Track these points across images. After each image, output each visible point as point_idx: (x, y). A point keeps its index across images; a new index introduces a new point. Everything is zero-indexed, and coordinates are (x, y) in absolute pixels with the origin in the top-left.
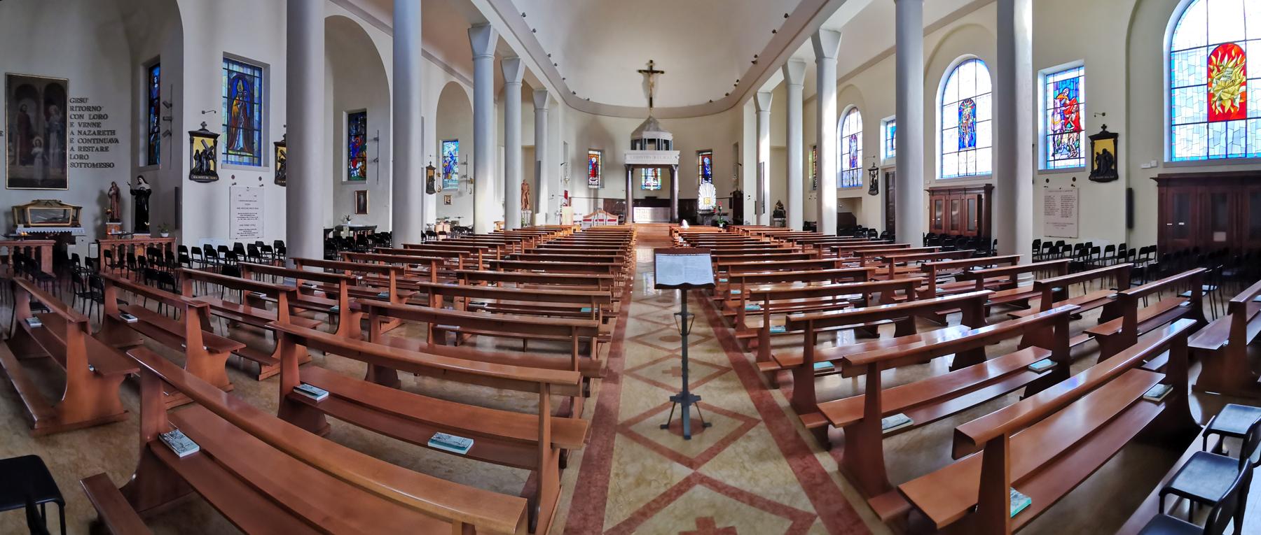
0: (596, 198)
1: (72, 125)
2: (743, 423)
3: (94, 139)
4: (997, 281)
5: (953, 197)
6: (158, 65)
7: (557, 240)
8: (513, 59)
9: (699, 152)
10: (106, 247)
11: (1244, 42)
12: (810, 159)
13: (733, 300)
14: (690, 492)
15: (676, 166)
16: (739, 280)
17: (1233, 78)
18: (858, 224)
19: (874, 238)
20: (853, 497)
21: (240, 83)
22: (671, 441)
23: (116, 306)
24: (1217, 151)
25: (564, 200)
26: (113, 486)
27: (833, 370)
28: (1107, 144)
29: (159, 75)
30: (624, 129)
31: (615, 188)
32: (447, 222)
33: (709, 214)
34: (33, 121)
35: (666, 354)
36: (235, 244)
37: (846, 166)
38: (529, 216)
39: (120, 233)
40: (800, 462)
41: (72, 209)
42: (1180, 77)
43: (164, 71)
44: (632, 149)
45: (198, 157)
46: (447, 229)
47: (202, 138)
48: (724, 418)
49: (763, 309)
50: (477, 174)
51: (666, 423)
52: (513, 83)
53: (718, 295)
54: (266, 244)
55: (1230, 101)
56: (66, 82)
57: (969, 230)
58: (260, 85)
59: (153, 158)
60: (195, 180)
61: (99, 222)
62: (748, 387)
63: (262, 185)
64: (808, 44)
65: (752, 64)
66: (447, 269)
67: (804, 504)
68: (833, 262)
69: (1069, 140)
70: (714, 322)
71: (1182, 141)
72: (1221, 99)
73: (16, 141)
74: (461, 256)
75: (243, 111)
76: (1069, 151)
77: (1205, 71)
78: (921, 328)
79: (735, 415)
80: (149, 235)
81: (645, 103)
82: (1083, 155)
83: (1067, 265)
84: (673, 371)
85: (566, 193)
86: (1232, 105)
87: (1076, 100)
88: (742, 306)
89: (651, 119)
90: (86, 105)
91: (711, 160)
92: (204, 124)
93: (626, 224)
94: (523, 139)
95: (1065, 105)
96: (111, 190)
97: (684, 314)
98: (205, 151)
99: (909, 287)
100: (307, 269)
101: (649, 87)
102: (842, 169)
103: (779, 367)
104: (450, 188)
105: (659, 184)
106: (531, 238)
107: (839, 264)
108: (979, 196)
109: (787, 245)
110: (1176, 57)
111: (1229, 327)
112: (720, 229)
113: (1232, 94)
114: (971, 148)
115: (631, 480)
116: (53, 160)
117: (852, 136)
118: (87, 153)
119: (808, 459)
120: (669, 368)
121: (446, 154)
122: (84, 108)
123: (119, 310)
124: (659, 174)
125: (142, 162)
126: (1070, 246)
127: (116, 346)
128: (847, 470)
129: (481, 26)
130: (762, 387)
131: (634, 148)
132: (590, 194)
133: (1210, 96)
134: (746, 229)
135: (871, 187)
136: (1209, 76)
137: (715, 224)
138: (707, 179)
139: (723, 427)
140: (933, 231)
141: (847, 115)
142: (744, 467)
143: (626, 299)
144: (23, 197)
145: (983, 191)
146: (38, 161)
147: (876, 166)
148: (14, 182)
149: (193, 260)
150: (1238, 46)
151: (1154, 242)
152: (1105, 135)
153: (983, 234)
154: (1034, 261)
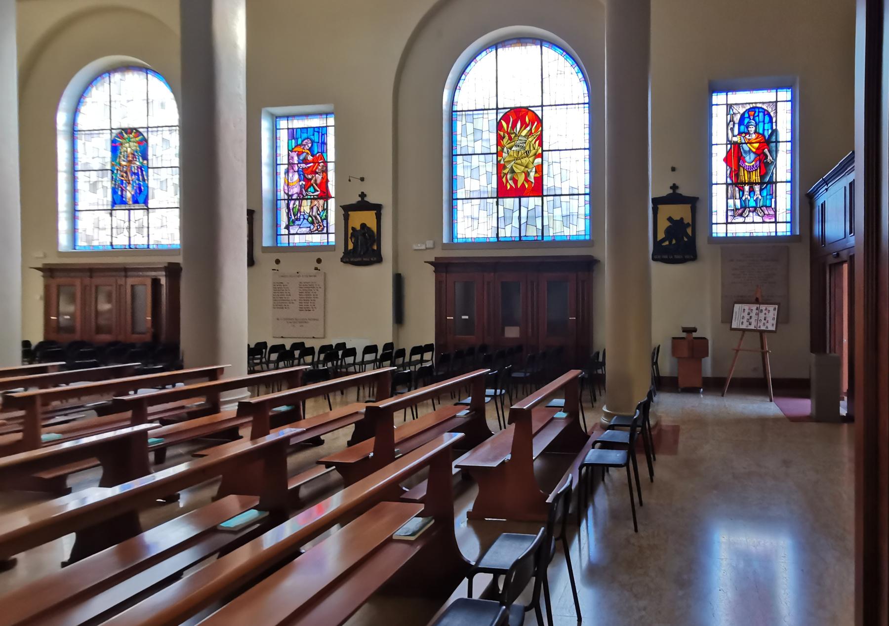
4: (183, 407)
5: (97, 280)
11: (540, 108)
17: (527, 148)
24: (508, 232)
28: (368, 218)
42: (463, 142)
55: (523, 174)
57: (133, 332)
69: (312, 208)
71: (466, 219)
72: (512, 171)
76: (312, 223)
77: (493, 138)
82: (332, 229)
83: (300, 375)
86: (526, 180)
87: (322, 157)
95: (305, 161)
108: (156, 282)
110: (459, 118)
111: (512, 439)
113: (526, 167)
114: (137, 206)
126: (312, 349)
133: (500, 167)
136: (498, 144)
140: (53, 337)
145: (164, 273)
150: (533, 112)
151: (431, 339)
152: (363, 205)
154: (250, 372)
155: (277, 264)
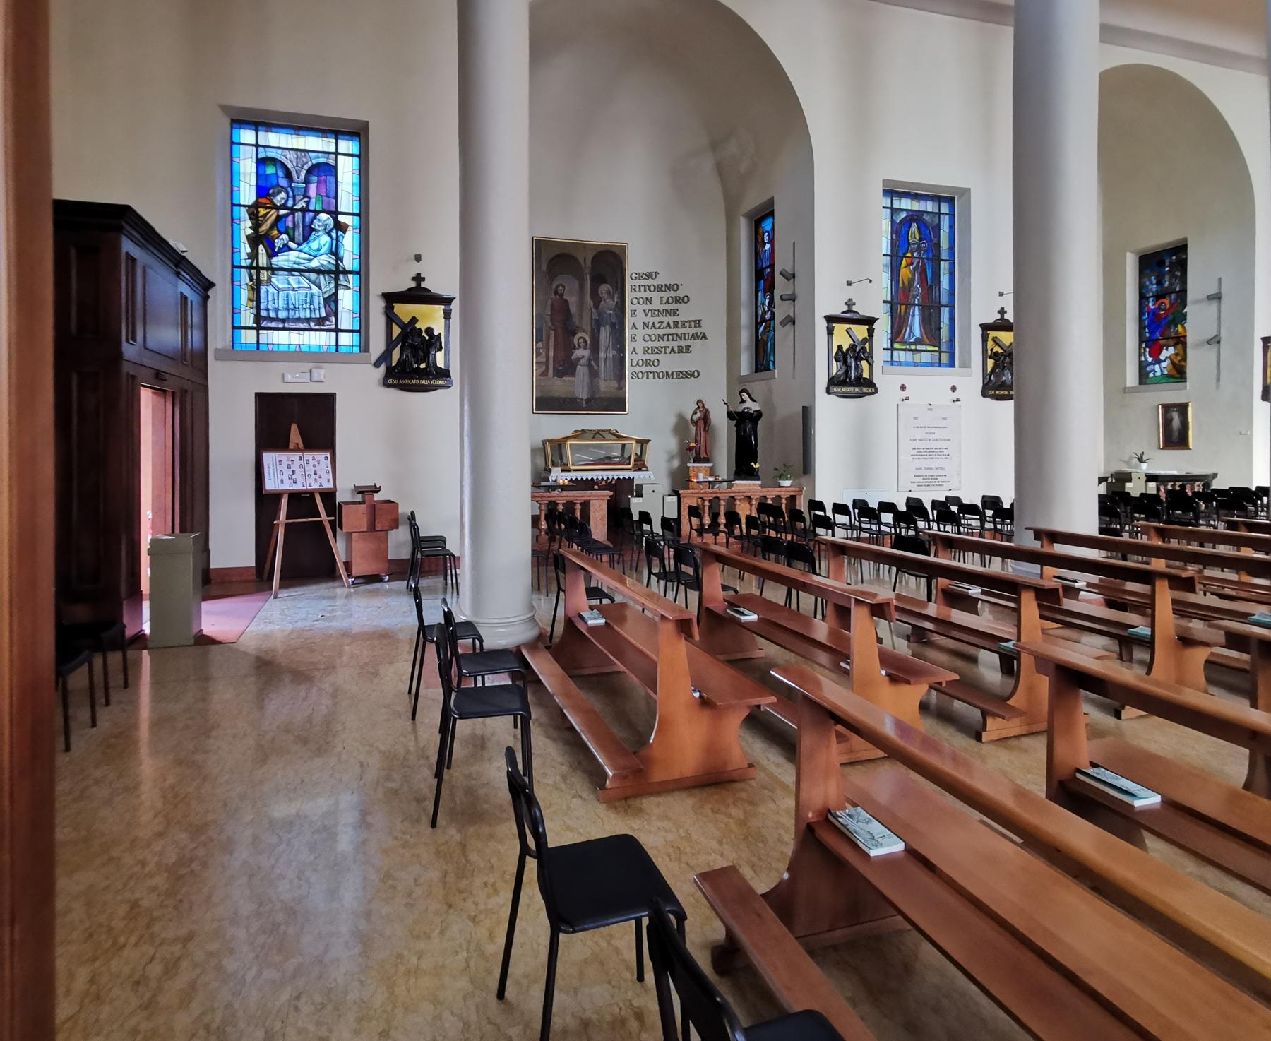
1: (634, 313)
3: (668, 335)
6: (772, 214)
10: (689, 501)
18: (1127, 707)
21: (914, 227)
23: (721, 595)
26: (751, 890)
29: (773, 228)
34: (573, 309)
36: (908, 500)
39: (711, 479)
41: (634, 443)
43: (781, 223)
45: (842, 356)
47: (847, 326)
54: (965, 501)
56: (623, 249)
58: (952, 227)
59: (763, 358)
60: (836, 394)
61: (676, 463)
63: (958, 400)
73: (548, 338)
75: (920, 274)
80: (759, 482)
90: (655, 282)
92: (850, 304)
96: (695, 413)
98: (852, 347)
100: (1061, 549)
116: (604, 368)
118: (656, 356)
122: (652, 288)
123: (725, 600)
125: (745, 367)
127: (720, 657)
144: (559, 425)
146: (581, 370)
148: (545, 403)
149: (835, 524)
155: (954, 386)
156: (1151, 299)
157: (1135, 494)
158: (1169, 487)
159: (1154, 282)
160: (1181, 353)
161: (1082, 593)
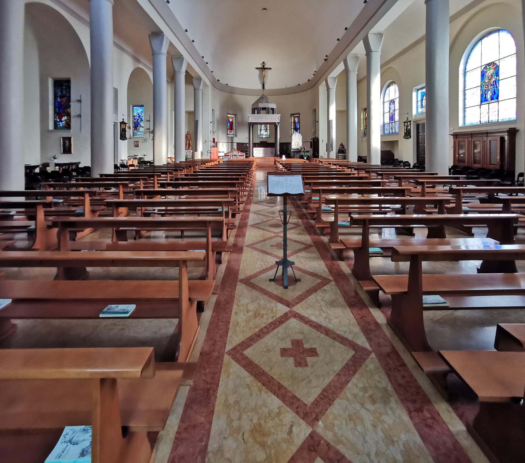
0: (232, 143)
2: (321, 281)
5: (474, 139)
7: (207, 168)
8: (180, 58)
9: (292, 115)
12: (362, 117)
13: (313, 203)
14: (288, 322)
15: (278, 123)
16: (318, 191)
18: (395, 158)
19: (408, 167)
20: (400, 347)
22: (276, 289)
25: (213, 144)
27: (382, 254)
30: (248, 102)
31: (242, 137)
32: (136, 158)
33: (298, 151)
35: (273, 235)
37: (387, 120)
38: (191, 153)
40: (359, 312)
44: (252, 114)
46: (136, 163)
48: (309, 277)
49: (334, 210)
50: (155, 127)
51: (273, 278)
52: (180, 72)
53: (304, 200)
57: (491, 164)
62: (323, 257)
64: (361, 44)
65: (324, 61)
66: (133, 189)
67: (362, 341)
68: (380, 182)
70: (301, 216)
74: (141, 180)
78: (448, 234)
79: (314, 275)
81: (260, 87)
84: (277, 246)
85: (214, 139)
88: (320, 207)
89: (264, 96)
91: (299, 120)
93: (250, 158)
94: (186, 107)
97: (285, 212)
99: (440, 204)
101: (263, 79)
102: (384, 122)
103: (344, 247)
104: (138, 136)
105: (268, 134)
106: (190, 167)
107: (384, 184)
108: (502, 139)
109: (348, 171)
112: (305, 160)
115: (251, 314)
117: (391, 101)
119: (364, 311)
120: (274, 244)
121: (135, 114)
124: (268, 128)
128: (392, 323)
129: (157, 34)
130: (333, 259)
131: (253, 113)
132: (228, 140)
134: (321, 160)
135: (406, 133)
137: (302, 157)
138: (297, 131)
139: (307, 283)
140: (457, 164)
141: (388, 87)
142: (322, 310)
143: (249, 202)
145: (507, 134)
147: (409, 119)
153: (506, 168)
156: (59, 98)
157: (49, 171)
158: (64, 168)
159: (60, 91)
160: (69, 118)
161: (15, 216)
